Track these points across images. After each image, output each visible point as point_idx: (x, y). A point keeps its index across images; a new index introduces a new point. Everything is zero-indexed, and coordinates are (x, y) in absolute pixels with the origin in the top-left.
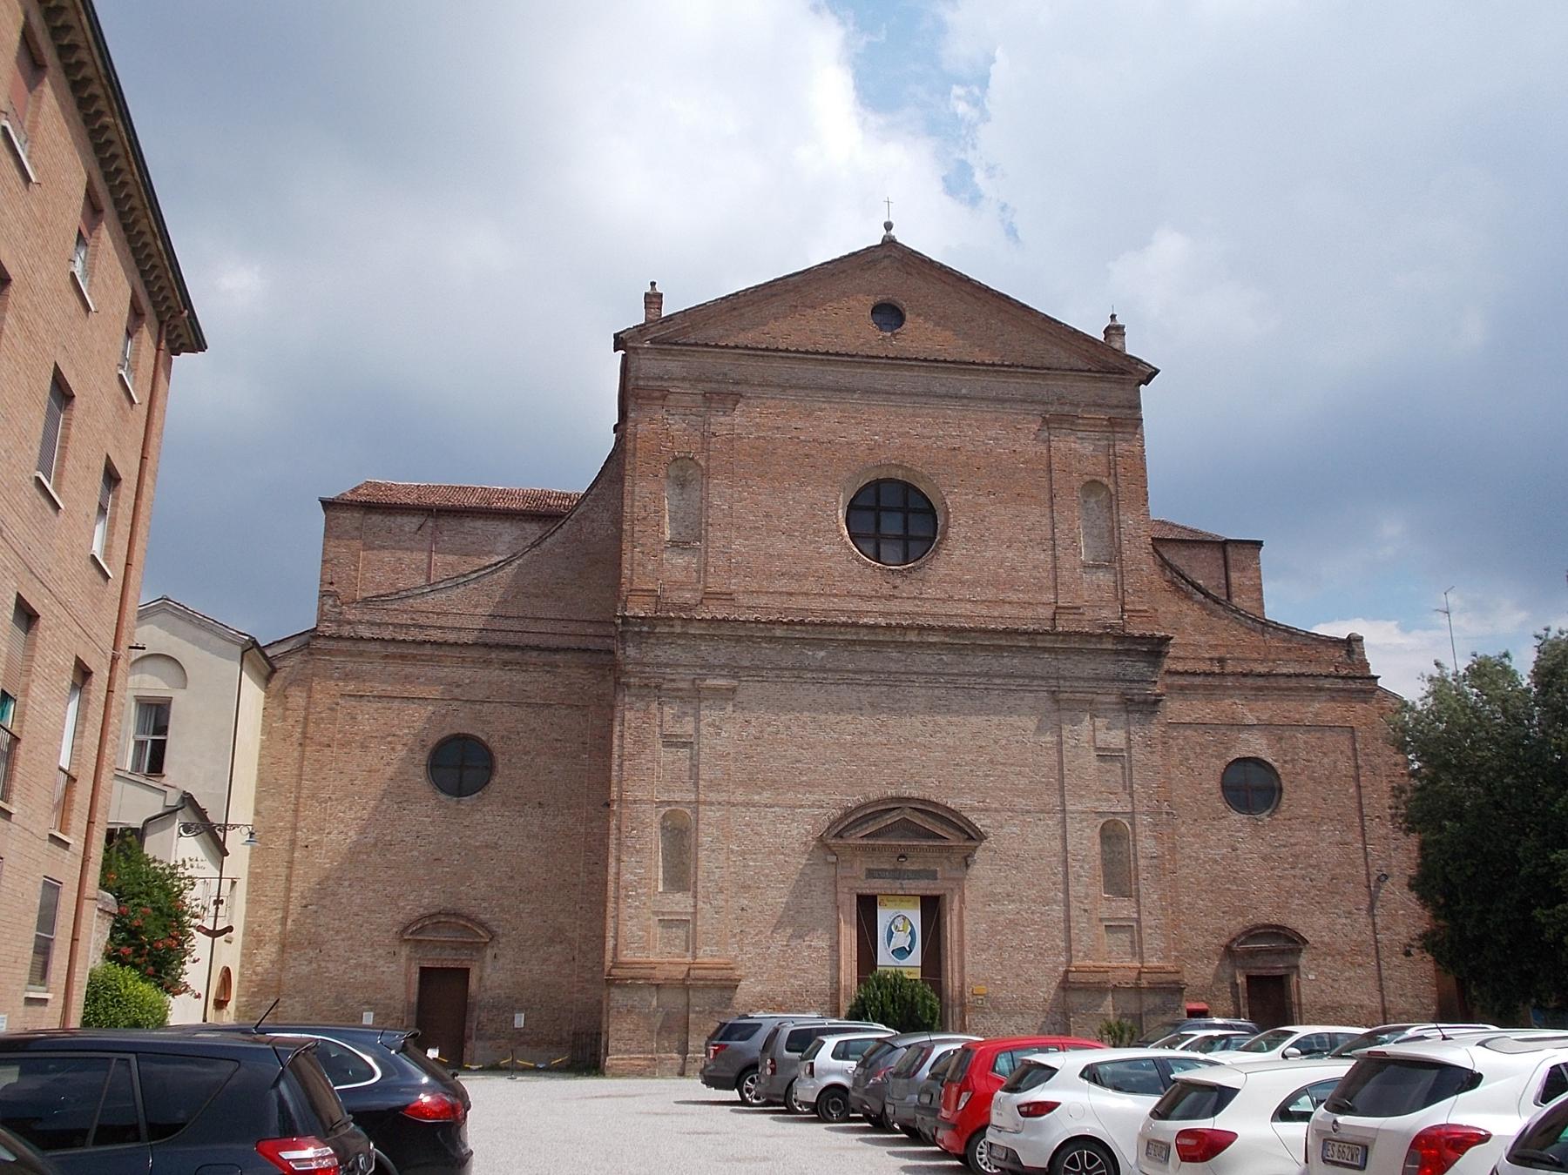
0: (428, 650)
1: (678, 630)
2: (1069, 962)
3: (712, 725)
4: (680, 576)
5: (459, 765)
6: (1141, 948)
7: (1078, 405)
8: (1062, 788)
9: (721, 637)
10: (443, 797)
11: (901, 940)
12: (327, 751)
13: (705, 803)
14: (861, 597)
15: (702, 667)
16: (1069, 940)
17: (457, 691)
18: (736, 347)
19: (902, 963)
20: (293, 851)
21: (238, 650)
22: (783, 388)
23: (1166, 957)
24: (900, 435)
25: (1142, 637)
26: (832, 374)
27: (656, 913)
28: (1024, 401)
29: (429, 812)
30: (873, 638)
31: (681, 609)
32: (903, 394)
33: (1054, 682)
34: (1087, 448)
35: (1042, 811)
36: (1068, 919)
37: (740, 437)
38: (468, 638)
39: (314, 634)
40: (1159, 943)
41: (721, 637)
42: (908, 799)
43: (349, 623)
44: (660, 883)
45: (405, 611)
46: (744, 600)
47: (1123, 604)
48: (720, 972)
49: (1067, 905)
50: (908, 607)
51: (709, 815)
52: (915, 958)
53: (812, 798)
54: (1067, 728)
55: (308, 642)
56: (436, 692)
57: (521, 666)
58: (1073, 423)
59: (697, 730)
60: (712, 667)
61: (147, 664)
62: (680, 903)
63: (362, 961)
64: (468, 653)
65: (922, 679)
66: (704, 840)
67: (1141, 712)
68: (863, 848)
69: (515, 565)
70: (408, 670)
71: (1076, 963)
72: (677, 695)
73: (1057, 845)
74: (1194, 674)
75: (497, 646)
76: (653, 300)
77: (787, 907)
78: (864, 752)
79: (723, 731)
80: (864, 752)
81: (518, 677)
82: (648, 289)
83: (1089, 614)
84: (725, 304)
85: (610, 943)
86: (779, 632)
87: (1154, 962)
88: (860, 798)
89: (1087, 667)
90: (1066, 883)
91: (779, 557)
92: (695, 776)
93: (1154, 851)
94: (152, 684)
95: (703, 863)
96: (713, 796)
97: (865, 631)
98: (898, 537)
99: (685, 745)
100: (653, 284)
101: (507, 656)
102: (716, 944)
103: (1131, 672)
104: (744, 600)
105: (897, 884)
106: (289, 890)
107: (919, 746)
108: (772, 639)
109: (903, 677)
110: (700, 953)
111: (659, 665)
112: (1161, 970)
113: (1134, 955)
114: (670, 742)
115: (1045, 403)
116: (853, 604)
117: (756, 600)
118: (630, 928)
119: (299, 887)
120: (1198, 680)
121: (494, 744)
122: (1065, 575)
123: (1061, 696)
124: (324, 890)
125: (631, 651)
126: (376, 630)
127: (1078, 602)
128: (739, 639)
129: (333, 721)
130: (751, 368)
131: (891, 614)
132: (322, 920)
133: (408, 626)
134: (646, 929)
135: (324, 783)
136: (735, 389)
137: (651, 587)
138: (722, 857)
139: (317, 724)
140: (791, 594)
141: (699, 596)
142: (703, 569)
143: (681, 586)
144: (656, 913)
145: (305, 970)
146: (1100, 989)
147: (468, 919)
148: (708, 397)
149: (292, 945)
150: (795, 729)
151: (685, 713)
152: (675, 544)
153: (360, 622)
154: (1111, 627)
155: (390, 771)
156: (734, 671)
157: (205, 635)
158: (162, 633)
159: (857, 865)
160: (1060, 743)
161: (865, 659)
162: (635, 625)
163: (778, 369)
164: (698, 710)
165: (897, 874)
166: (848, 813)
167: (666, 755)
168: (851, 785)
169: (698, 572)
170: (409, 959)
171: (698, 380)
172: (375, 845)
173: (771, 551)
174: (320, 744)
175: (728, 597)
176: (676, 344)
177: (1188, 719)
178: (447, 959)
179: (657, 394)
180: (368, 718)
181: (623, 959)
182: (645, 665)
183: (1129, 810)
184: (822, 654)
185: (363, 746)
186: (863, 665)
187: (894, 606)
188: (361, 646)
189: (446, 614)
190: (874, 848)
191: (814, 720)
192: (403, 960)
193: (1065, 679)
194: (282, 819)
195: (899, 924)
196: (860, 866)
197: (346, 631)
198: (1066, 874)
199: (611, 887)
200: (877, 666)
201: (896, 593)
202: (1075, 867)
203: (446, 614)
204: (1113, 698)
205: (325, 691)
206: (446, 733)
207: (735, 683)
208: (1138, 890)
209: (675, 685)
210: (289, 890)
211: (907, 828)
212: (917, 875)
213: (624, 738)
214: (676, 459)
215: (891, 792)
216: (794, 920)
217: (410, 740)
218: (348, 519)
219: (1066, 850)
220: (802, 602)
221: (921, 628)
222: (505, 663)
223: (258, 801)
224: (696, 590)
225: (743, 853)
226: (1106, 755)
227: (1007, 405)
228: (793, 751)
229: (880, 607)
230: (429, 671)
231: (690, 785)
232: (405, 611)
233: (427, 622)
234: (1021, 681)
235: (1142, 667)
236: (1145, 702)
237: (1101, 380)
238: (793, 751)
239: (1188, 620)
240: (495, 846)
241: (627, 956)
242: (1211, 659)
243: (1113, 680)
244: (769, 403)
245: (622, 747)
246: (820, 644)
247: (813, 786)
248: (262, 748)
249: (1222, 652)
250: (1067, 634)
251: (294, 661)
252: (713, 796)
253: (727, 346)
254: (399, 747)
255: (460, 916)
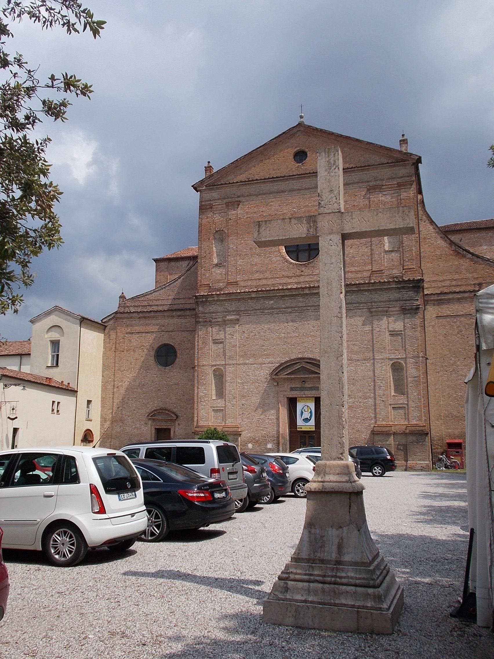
0: (152, 314)
1: (216, 299)
2: (376, 422)
3: (230, 334)
4: (219, 277)
5: (165, 355)
6: (408, 416)
7: (383, 180)
8: (373, 349)
9: (232, 300)
10: (160, 367)
11: (306, 415)
12: (122, 353)
13: (228, 364)
14: (288, 277)
15: (226, 312)
16: (375, 413)
17: (163, 328)
18: (237, 182)
19: (307, 424)
20: (114, 389)
21: (78, 321)
22: (257, 195)
23: (420, 420)
24: (304, 207)
25: (409, 280)
26: (275, 186)
27: (211, 407)
28: (358, 183)
29: (156, 372)
30: (290, 293)
31: (218, 290)
32: (306, 189)
33: (369, 304)
34: (389, 198)
35: (365, 360)
36: (375, 405)
37: (240, 218)
38: (166, 308)
39: (116, 313)
40: (417, 414)
41: (232, 300)
42: (304, 358)
43: (128, 307)
44: (393, 391)
45: (145, 301)
46: (242, 284)
47: (403, 266)
48: (234, 429)
49: (375, 399)
50: (307, 279)
51: (230, 369)
52: (312, 422)
53: (269, 360)
54: (376, 322)
55: (116, 316)
56: (156, 328)
57: (185, 316)
58: (381, 188)
59: (225, 337)
60: (229, 312)
61: (53, 329)
62: (220, 403)
63: (136, 426)
64: (166, 314)
65: (313, 308)
66: (228, 379)
67: (410, 313)
68: (284, 379)
69: (182, 278)
70: (147, 322)
71: (378, 423)
72: (217, 324)
73: (371, 374)
74: (465, 292)
75: (175, 310)
76: (208, 168)
77: (260, 404)
78: (289, 340)
79: (235, 336)
80: (289, 340)
81: (183, 321)
82: (206, 165)
83: (387, 273)
84: (233, 165)
85: (196, 419)
86: (253, 295)
87: (414, 422)
88: (288, 359)
89: (385, 296)
90: (375, 390)
91: (256, 265)
92: (225, 354)
93: (416, 374)
94: (54, 335)
95: (227, 388)
96: (231, 362)
97: (287, 291)
98: (306, 250)
99: (221, 343)
100: (209, 162)
101: (179, 313)
102: (233, 418)
103: (406, 296)
104: (242, 284)
105: (303, 393)
106: (113, 402)
107: (311, 336)
108: (252, 298)
109: (305, 308)
110: (227, 422)
111: (210, 313)
112: (416, 425)
113: (405, 419)
114: (215, 342)
115: (368, 182)
116: (284, 281)
117: (247, 285)
118: (202, 413)
119: (116, 401)
120: (466, 295)
121: (176, 347)
122: (376, 257)
123: (372, 310)
124: (123, 402)
125: (201, 309)
126: (136, 308)
127: (383, 268)
128: (239, 300)
129: (124, 343)
130: (244, 190)
131: (300, 283)
132: (124, 412)
133: (146, 306)
134: (208, 413)
135: (122, 364)
136: (239, 199)
137: (208, 283)
138: (235, 385)
139: (119, 344)
140: (260, 279)
141: (225, 284)
142: (227, 274)
143: (219, 281)
144: (211, 407)
145: (119, 430)
146: (387, 434)
147: (169, 411)
148: (228, 205)
149: (115, 421)
150: (262, 333)
151: (220, 331)
152: (217, 265)
153: (131, 306)
154: (396, 277)
155: (142, 359)
156: (238, 312)
157: (69, 317)
158: (57, 318)
159: (286, 386)
160: (372, 330)
161: (289, 302)
162: (200, 298)
163: (254, 188)
164: (225, 329)
165: (302, 389)
166: (281, 364)
167: (213, 347)
168: (284, 354)
169: (225, 275)
170: (151, 425)
171: (224, 198)
172: (139, 386)
173: (252, 263)
174: (120, 351)
175: (236, 283)
176: (215, 185)
177: (462, 313)
178: (163, 425)
179: (208, 207)
180: (135, 340)
181: (200, 425)
182: (205, 313)
183: (404, 356)
184: (272, 302)
185: (134, 351)
186: (288, 305)
187: (302, 279)
188: (131, 315)
189: (159, 300)
190: (292, 379)
191: (269, 329)
192: (149, 426)
193: (375, 302)
194: (110, 378)
195: (305, 409)
196: (287, 386)
197: (127, 310)
198: (375, 386)
199: (196, 398)
200: (293, 305)
201: (302, 273)
202: (379, 383)
203: (159, 300)
204: (397, 309)
205: (122, 330)
206: (160, 344)
207: (238, 317)
208: (407, 392)
209: (216, 320)
210: (113, 402)
211: (303, 370)
212: (311, 389)
213: (199, 343)
214: (217, 231)
215: (300, 356)
216: (263, 406)
217: (148, 347)
218: (163, 265)
219: (374, 376)
220: (264, 282)
221: (310, 288)
222: (179, 316)
223: (103, 372)
224: (224, 282)
225: (243, 383)
226: (393, 334)
227: (351, 186)
228: (261, 342)
229: (296, 280)
230: (153, 321)
231: (223, 358)
232: (145, 301)
233: (153, 304)
234: (355, 305)
235: (411, 293)
236: (411, 309)
237: (394, 166)
238: (261, 342)
239: (463, 267)
240: (178, 384)
241: (201, 423)
242: (474, 284)
243: (397, 301)
244: (251, 203)
245: (198, 345)
246: (270, 298)
247: (269, 355)
248: (103, 354)
249: (480, 280)
250: (375, 283)
251: (111, 322)
252: (231, 362)
253: (233, 183)
254: (145, 350)
255: (166, 410)
